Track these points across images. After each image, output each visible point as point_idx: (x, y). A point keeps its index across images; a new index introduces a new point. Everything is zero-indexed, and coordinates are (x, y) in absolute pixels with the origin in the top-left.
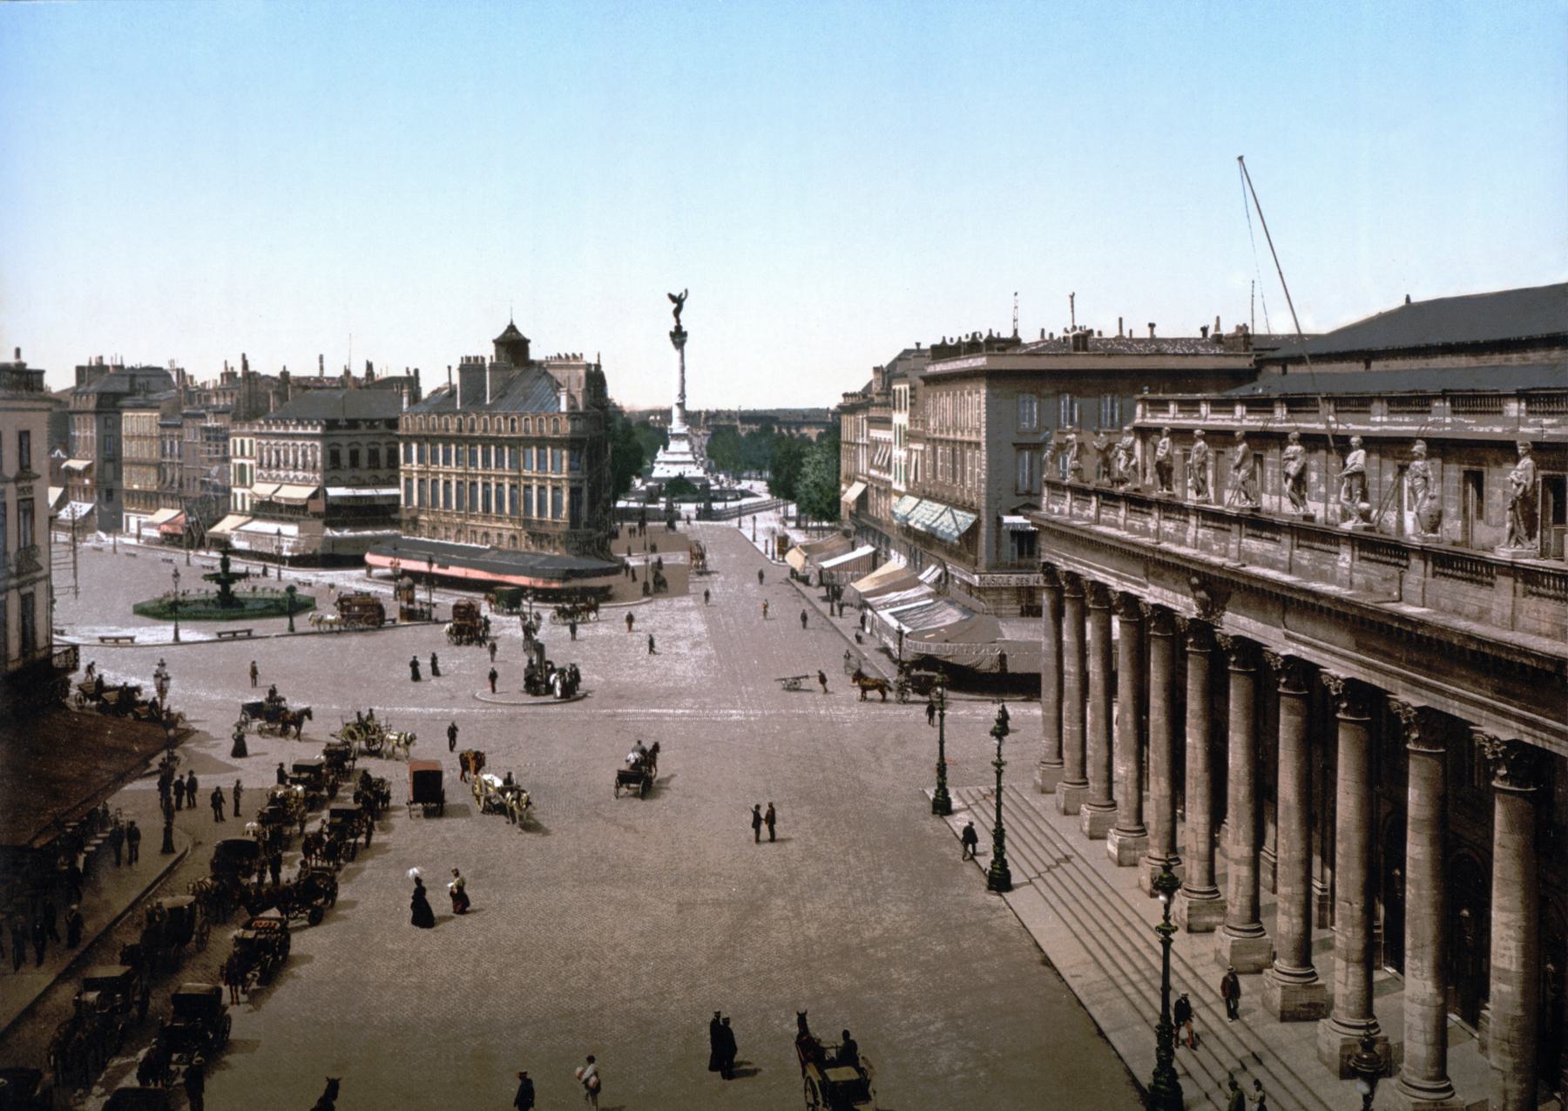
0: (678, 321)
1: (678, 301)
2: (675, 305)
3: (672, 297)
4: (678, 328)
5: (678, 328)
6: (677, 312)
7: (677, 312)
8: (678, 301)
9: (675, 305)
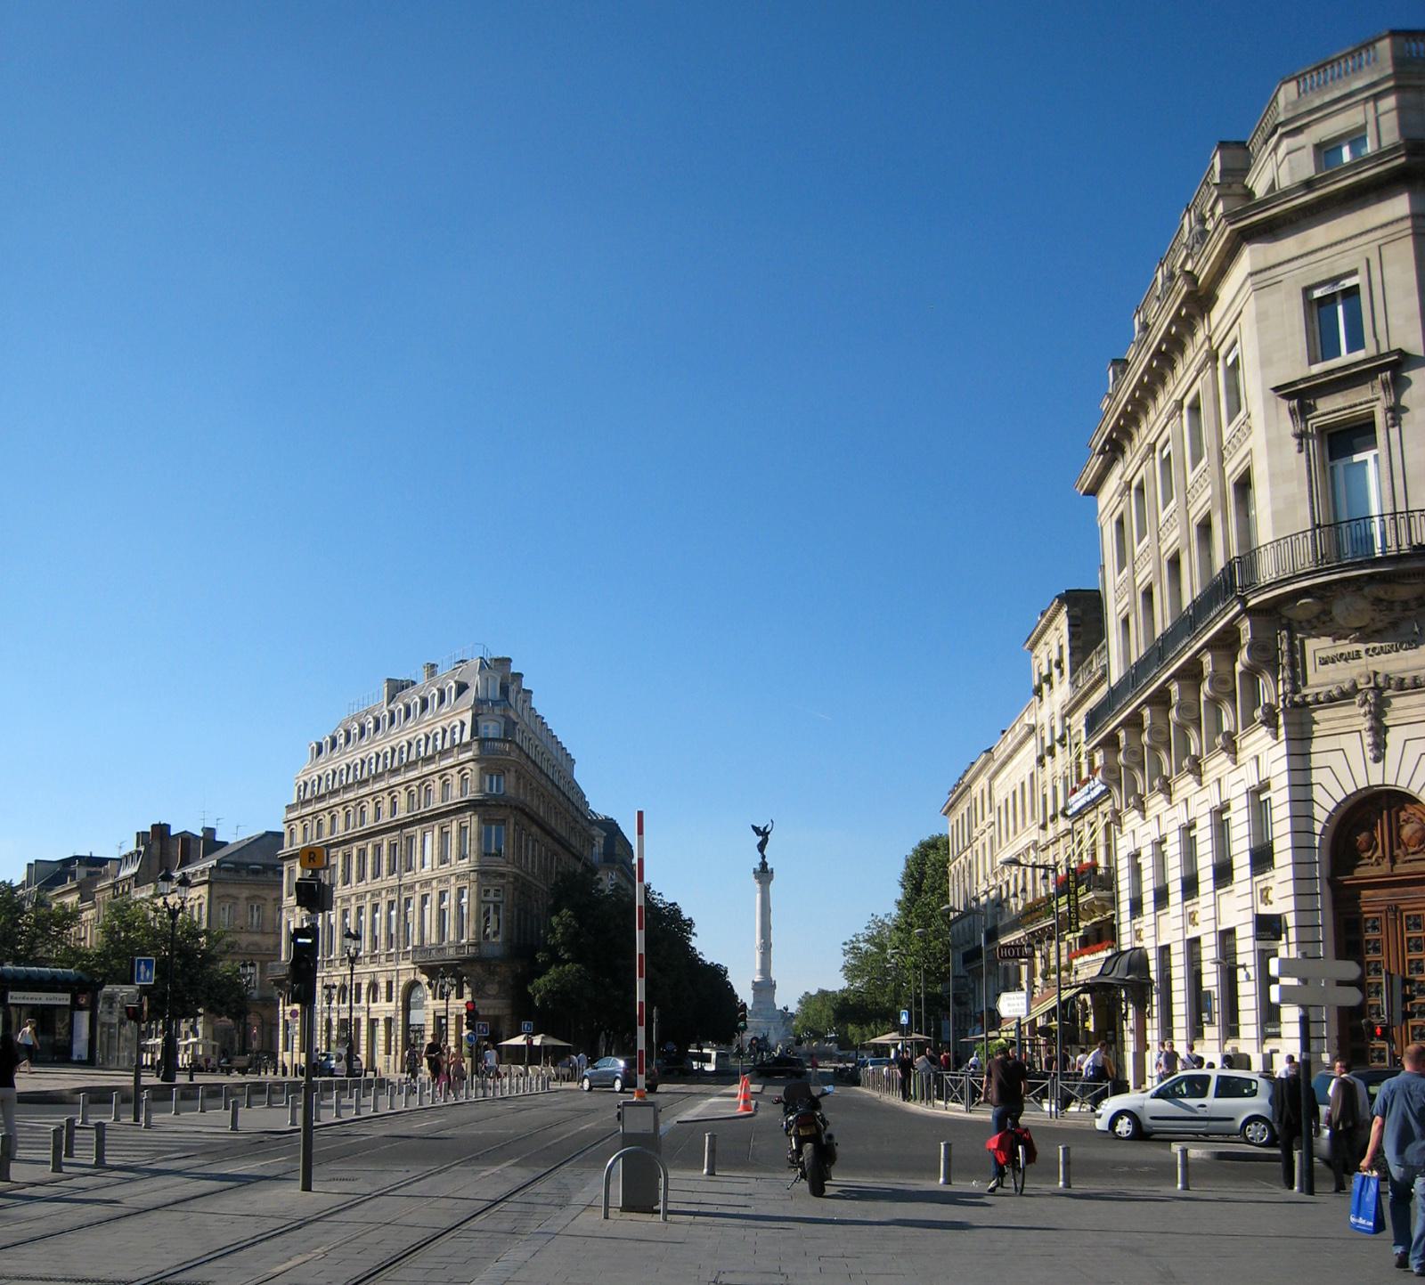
0: (764, 857)
1: (763, 834)
2: (760, 838)
3: (756, 829)
4: (764, 865)
5: (764, 865)
6: (762, 847)
7: (762, 847)
8: (763, 834)
9: (760, 838)
